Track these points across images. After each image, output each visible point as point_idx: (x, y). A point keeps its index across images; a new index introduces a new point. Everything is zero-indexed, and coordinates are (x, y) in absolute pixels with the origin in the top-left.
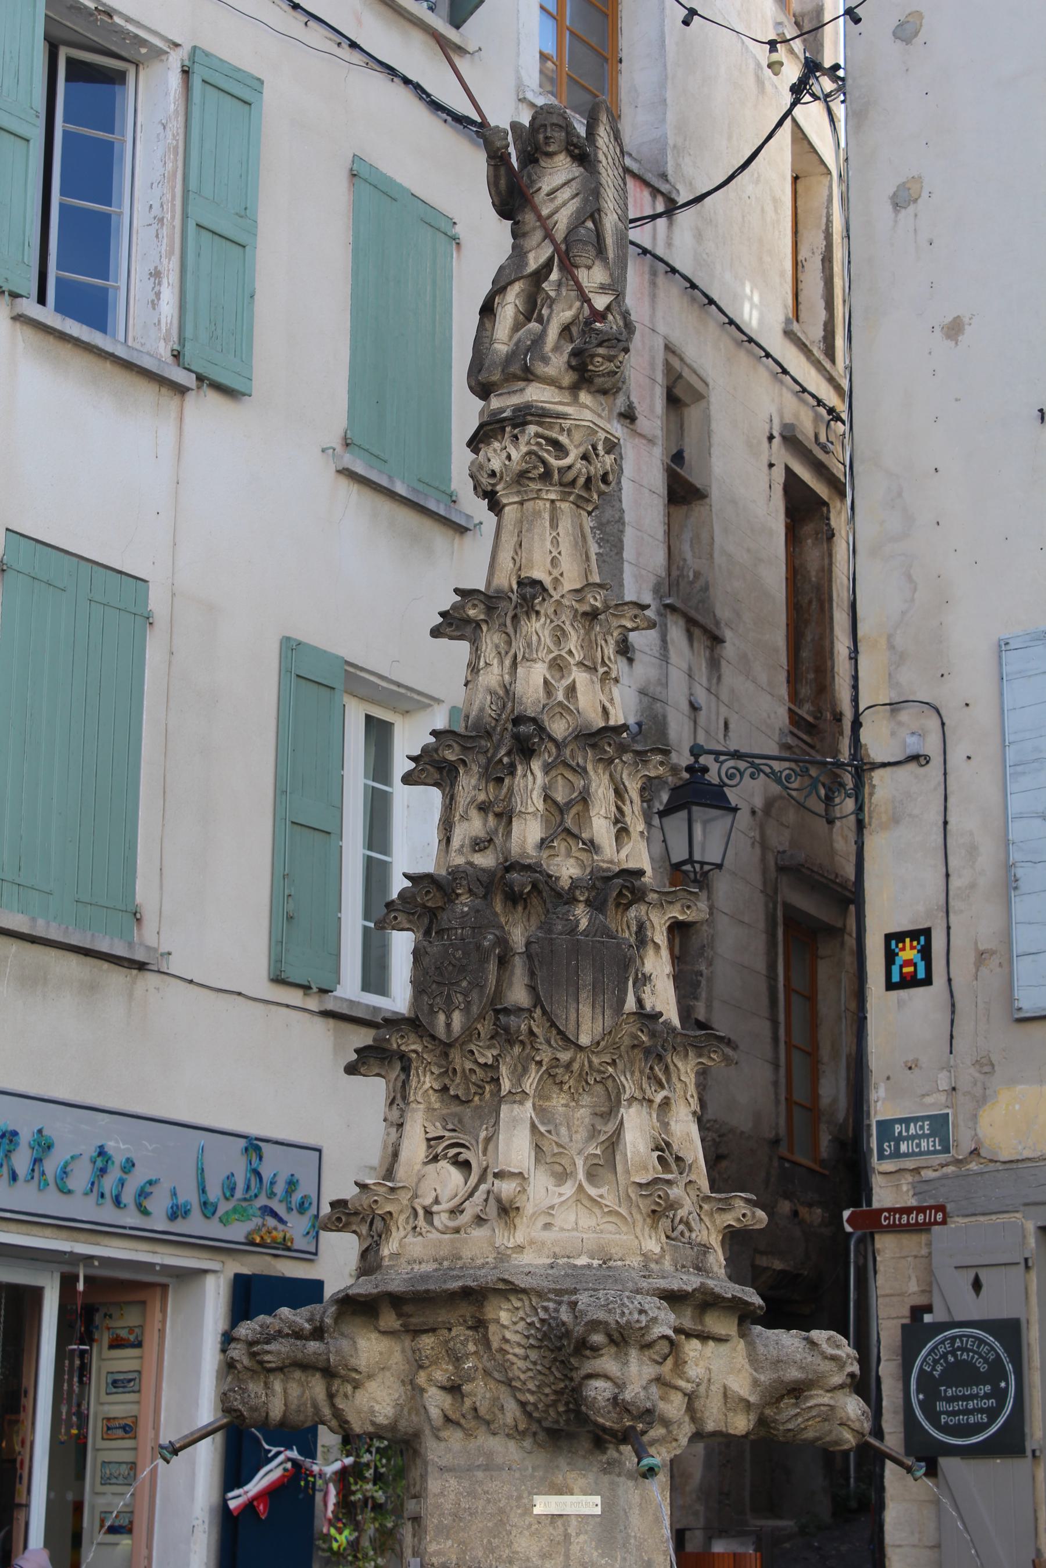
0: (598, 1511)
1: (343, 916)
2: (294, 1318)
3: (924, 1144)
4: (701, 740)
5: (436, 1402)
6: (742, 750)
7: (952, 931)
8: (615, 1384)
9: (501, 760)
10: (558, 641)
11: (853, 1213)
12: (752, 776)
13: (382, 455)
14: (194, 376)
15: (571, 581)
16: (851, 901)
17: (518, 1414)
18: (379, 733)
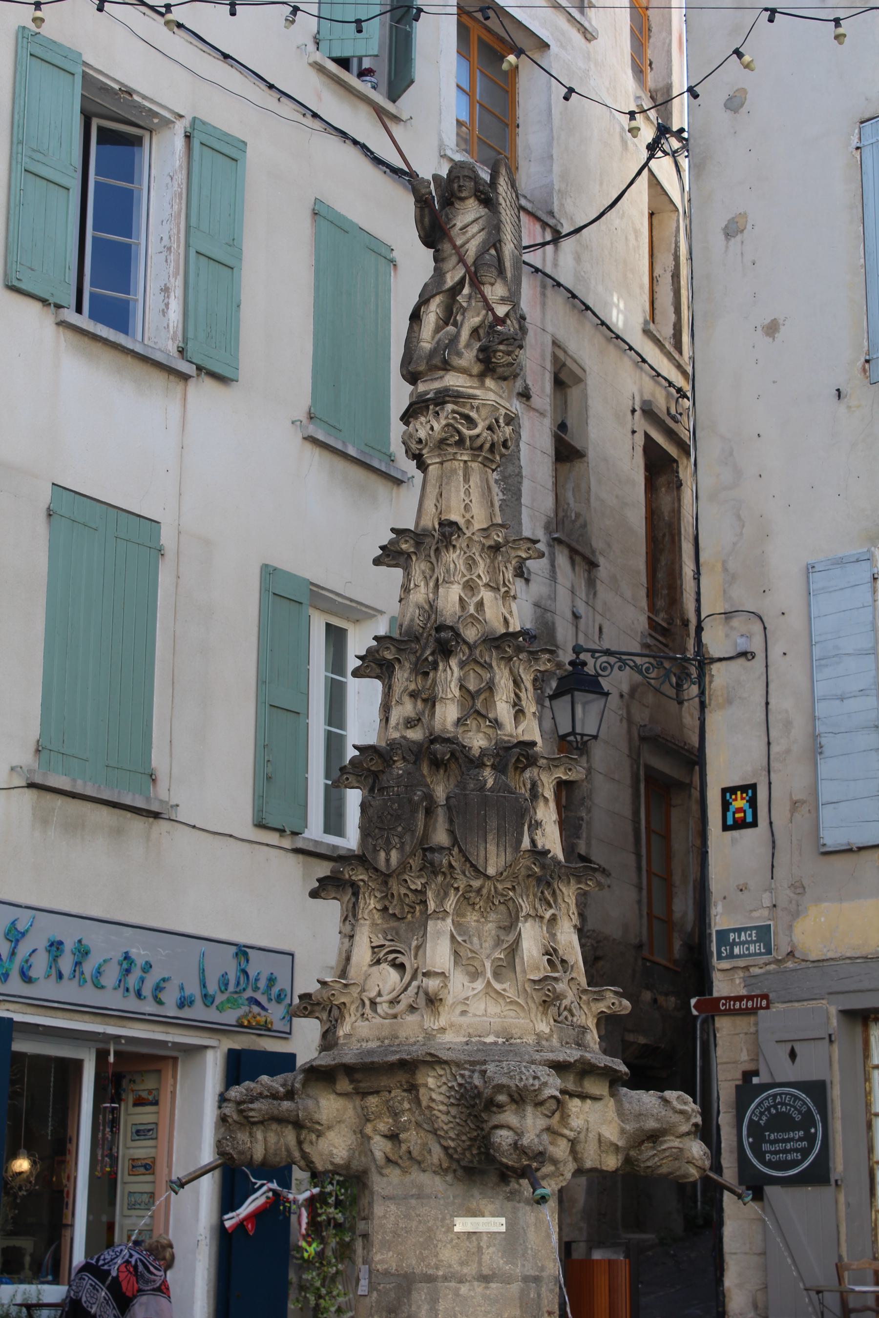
1: (309, 776)
2: (272, 1083)
3: (752, 948)
4: (581, 641)
5: (380, 1147)
6: (613, 649)
7: (772, 786)
8: (516, 1133)
9: (426, 659)
10: (470, 568)
11: (698, 1001)
12: (620, 668)
13: (338, 426)
14: (195, 367)
16: (696, 763)
17: (442, 1155)
18: (336, 637)
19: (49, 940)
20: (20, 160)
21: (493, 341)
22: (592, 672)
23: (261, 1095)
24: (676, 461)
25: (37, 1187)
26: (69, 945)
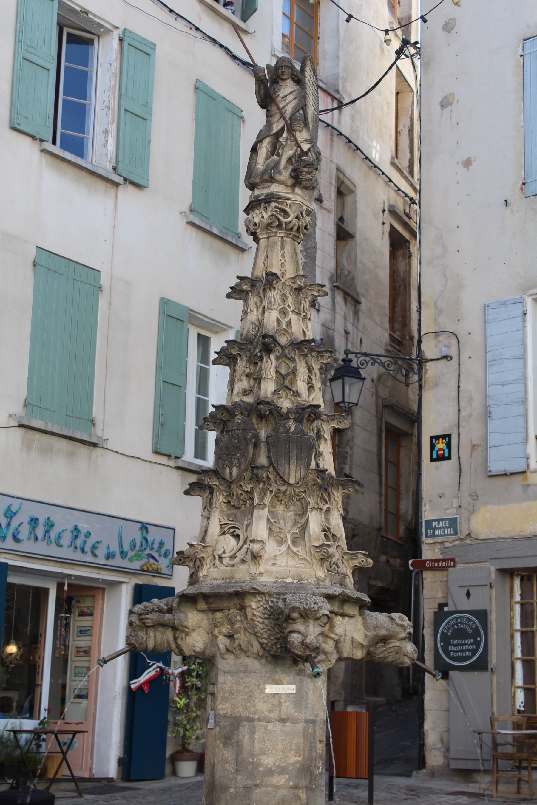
0: (294, 692)
1: (186, 424)
3: (446, 531)
4: (350, 347)
5: (223, 642)
6: (368, 352)
7: (461, 435)
8: (303, 635)
9: (256, 354)
12: (372, 364)
14: (122, 178)
15: (290, 273)
16: (416, 421)
17: (259, 648)
18: (204, 342)
19: (30, 517)
20: (20, 52)
21: (300, 166)
22: (355, 366)
23: (153, 610)
25: (21, 662)
26: (42, 521)
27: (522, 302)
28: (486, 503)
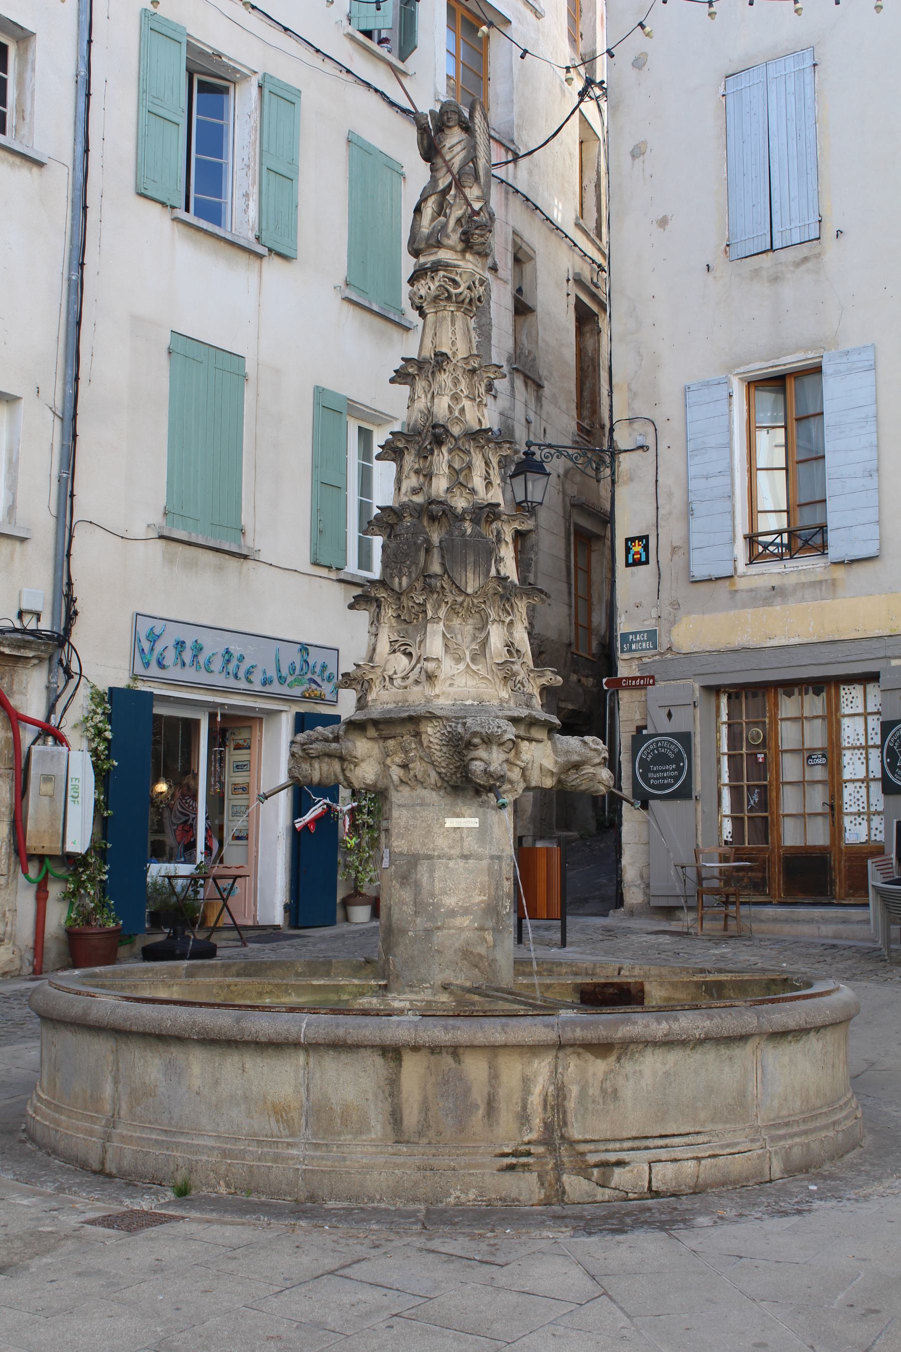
3: (644, 645)
4: (532, 439)
5: (396, 773)
10: (455, 385)
12: (558, 457)
15: (462, 353)
16: (608, 522)
18: (365, 435)
24: (597, 315)
27: (728, 382)
28: (689, 613)
